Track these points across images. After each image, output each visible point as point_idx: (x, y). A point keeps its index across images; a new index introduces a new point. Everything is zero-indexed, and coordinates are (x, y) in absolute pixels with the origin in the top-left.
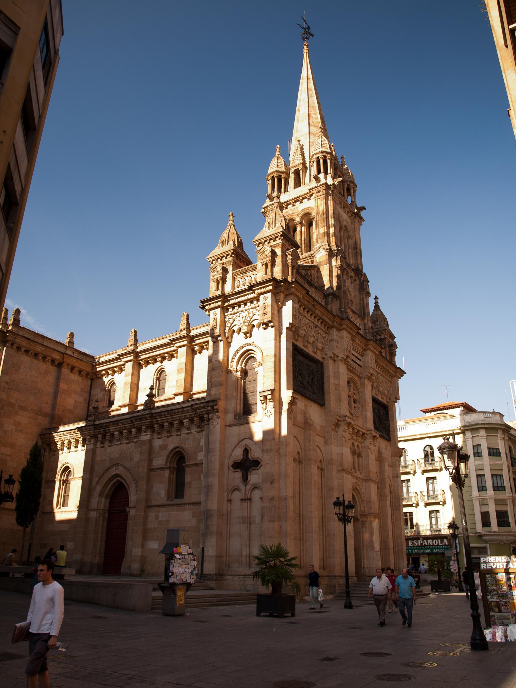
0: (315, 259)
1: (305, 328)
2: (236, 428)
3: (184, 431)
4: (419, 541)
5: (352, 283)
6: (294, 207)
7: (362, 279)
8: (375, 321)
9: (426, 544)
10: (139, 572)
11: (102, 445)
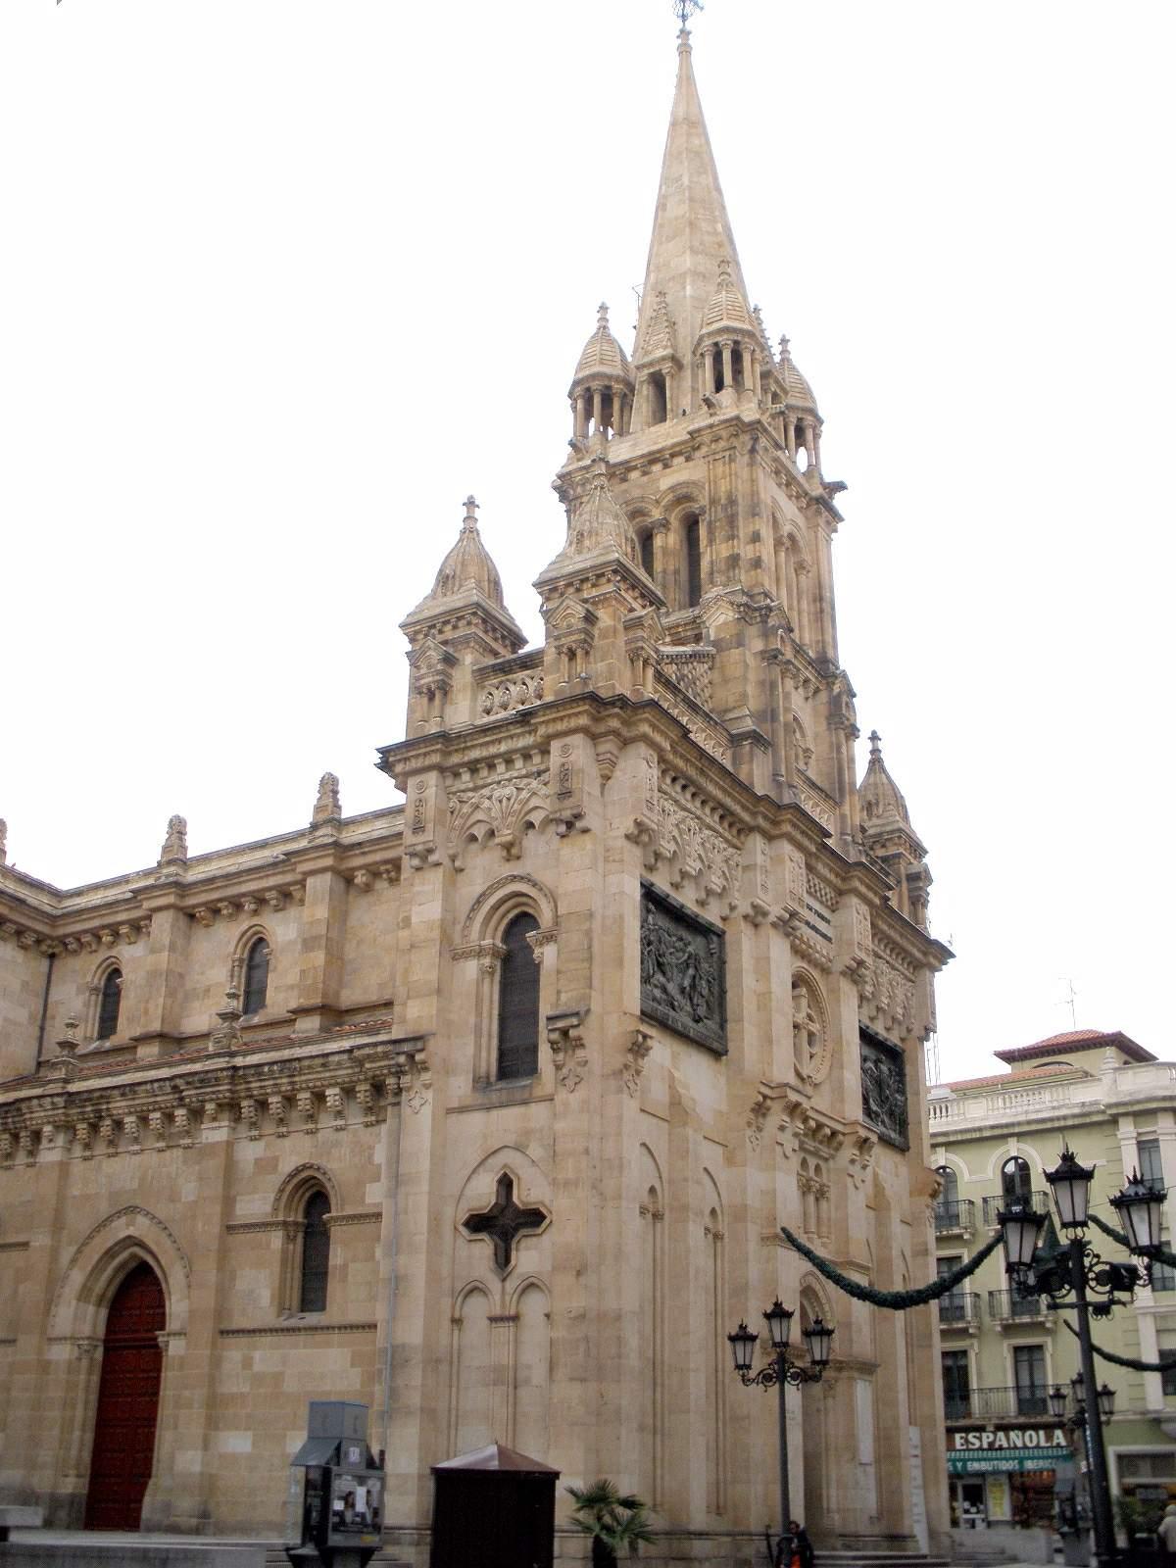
0: (704, 631)
1: (676, 833)
2: (477, 1119)
3: (327, 1121)
4: (984, 1435)
5: (807, 699)
6: (645, 478)
7: (836, 689)
8: (870, 804)
9: (1005, 1445)
10: (194, 1521)
11: (88, 1153)
